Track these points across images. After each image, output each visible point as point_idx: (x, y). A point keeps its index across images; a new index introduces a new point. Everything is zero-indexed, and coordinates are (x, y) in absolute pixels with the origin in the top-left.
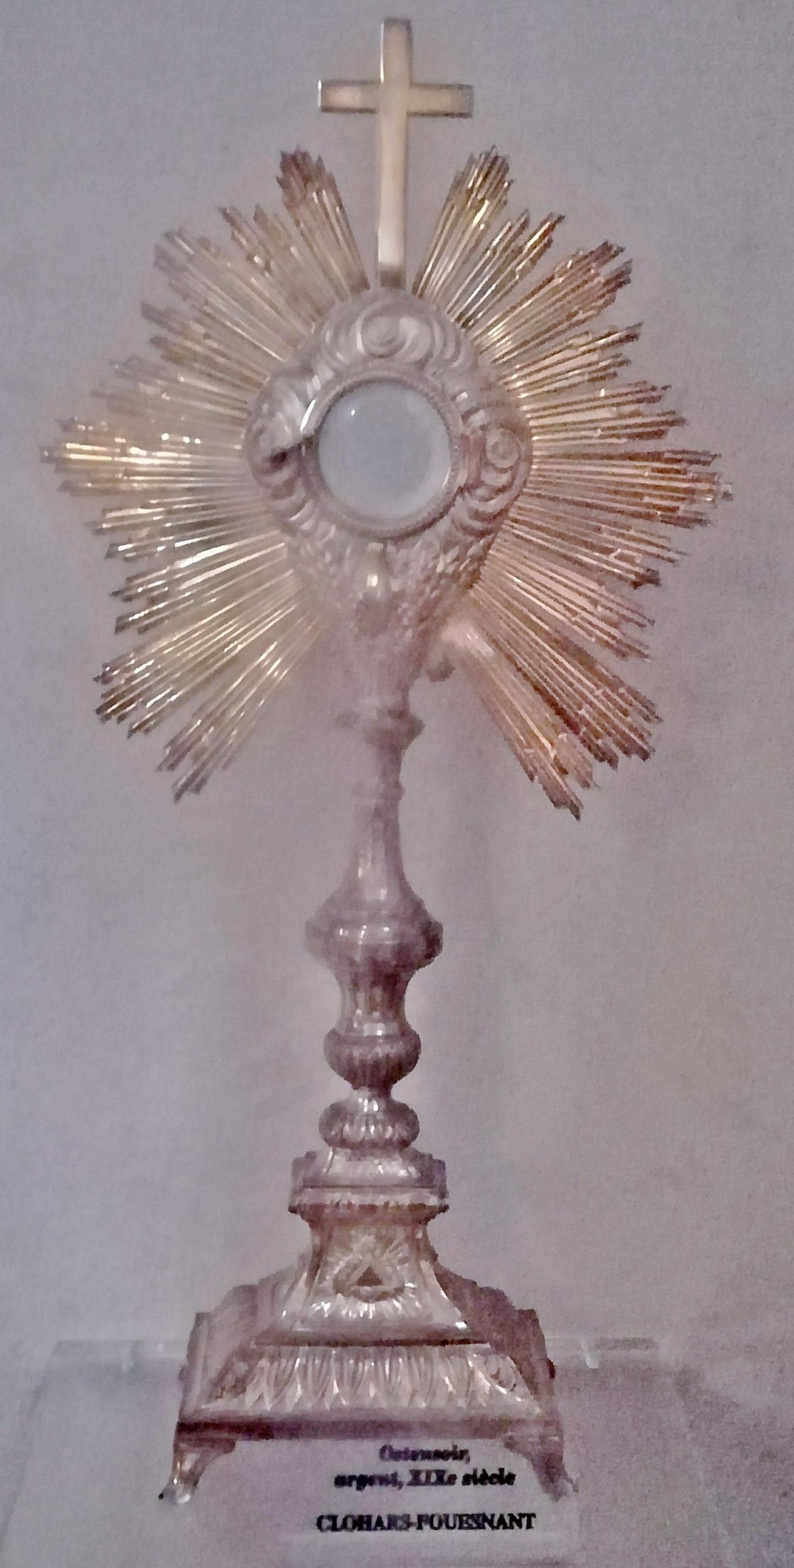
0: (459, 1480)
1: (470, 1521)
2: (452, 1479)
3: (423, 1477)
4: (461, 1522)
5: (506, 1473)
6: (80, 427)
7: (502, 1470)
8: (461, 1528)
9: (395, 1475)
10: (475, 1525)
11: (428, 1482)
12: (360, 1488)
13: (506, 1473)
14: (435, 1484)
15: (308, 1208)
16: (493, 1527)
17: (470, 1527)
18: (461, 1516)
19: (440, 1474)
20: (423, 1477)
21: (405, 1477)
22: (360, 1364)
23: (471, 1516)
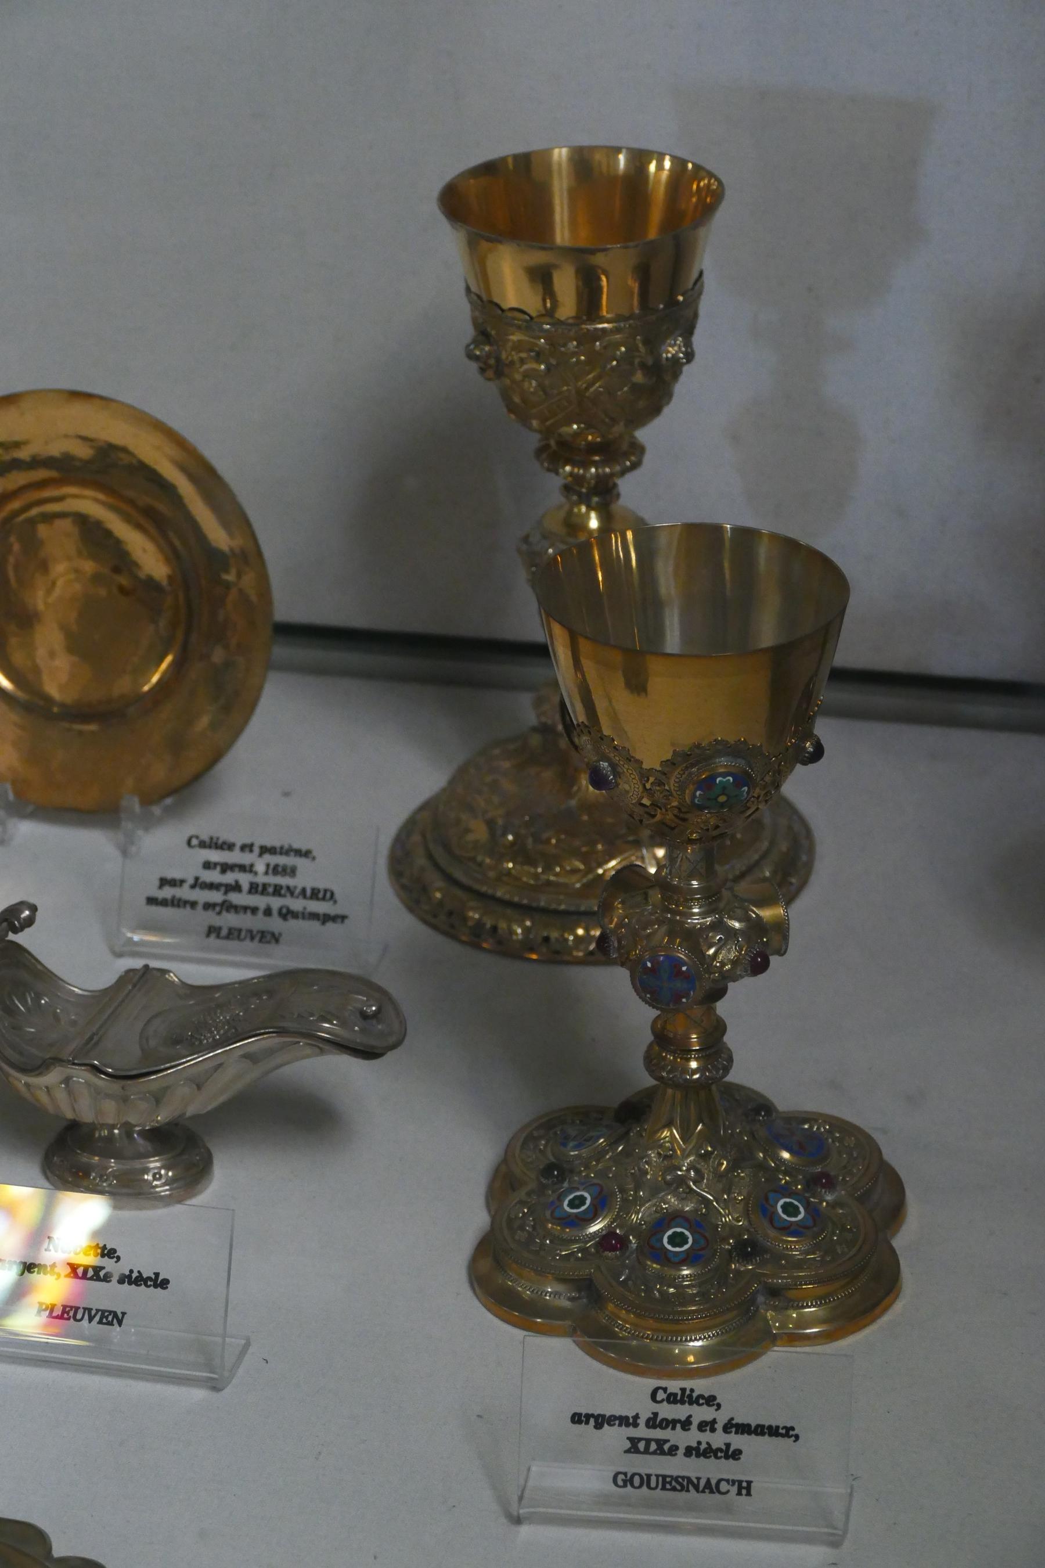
0: (681, 1451)
1: (674, 1483)
2: (673, 1450)
3: (641, 1446)
4: (664, 1483)
5: (161, 1278)
6: (471, 914)
7: (157, 1275)
8: (664, 1488)
9: (252, 866)
10: (679, 1487)
11: (647, 1451)
12: (598, 1426)
13: (161, 1278)
14: (654, 1453)
15: (510, 160)
16: (697, 1491)
17: (674, 1489)
18: (664, 1477)
19: (660, 1443)
20: (641, 1446)
21: (245, 887)
22: (735, 1312)
23: (676, 1479)
